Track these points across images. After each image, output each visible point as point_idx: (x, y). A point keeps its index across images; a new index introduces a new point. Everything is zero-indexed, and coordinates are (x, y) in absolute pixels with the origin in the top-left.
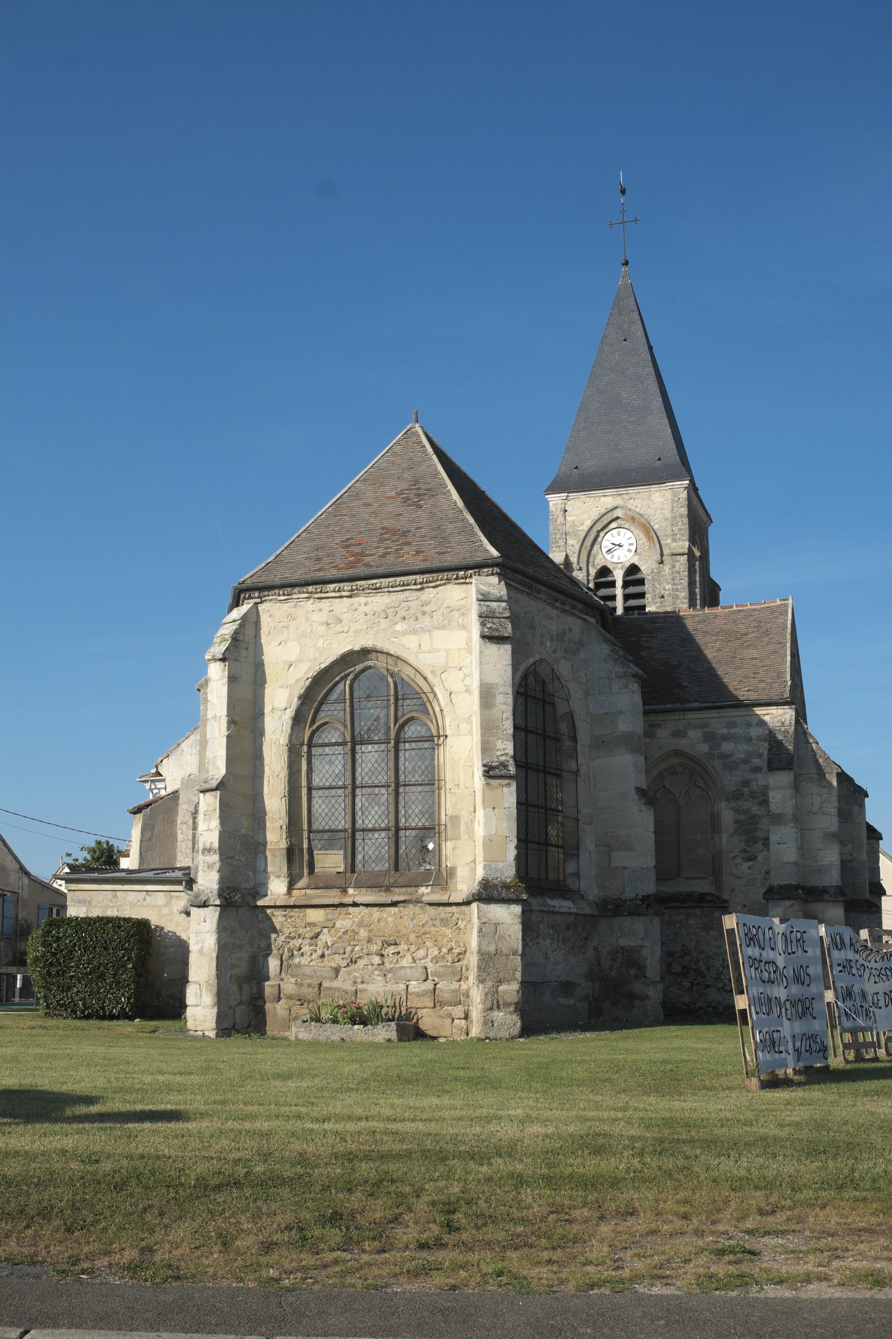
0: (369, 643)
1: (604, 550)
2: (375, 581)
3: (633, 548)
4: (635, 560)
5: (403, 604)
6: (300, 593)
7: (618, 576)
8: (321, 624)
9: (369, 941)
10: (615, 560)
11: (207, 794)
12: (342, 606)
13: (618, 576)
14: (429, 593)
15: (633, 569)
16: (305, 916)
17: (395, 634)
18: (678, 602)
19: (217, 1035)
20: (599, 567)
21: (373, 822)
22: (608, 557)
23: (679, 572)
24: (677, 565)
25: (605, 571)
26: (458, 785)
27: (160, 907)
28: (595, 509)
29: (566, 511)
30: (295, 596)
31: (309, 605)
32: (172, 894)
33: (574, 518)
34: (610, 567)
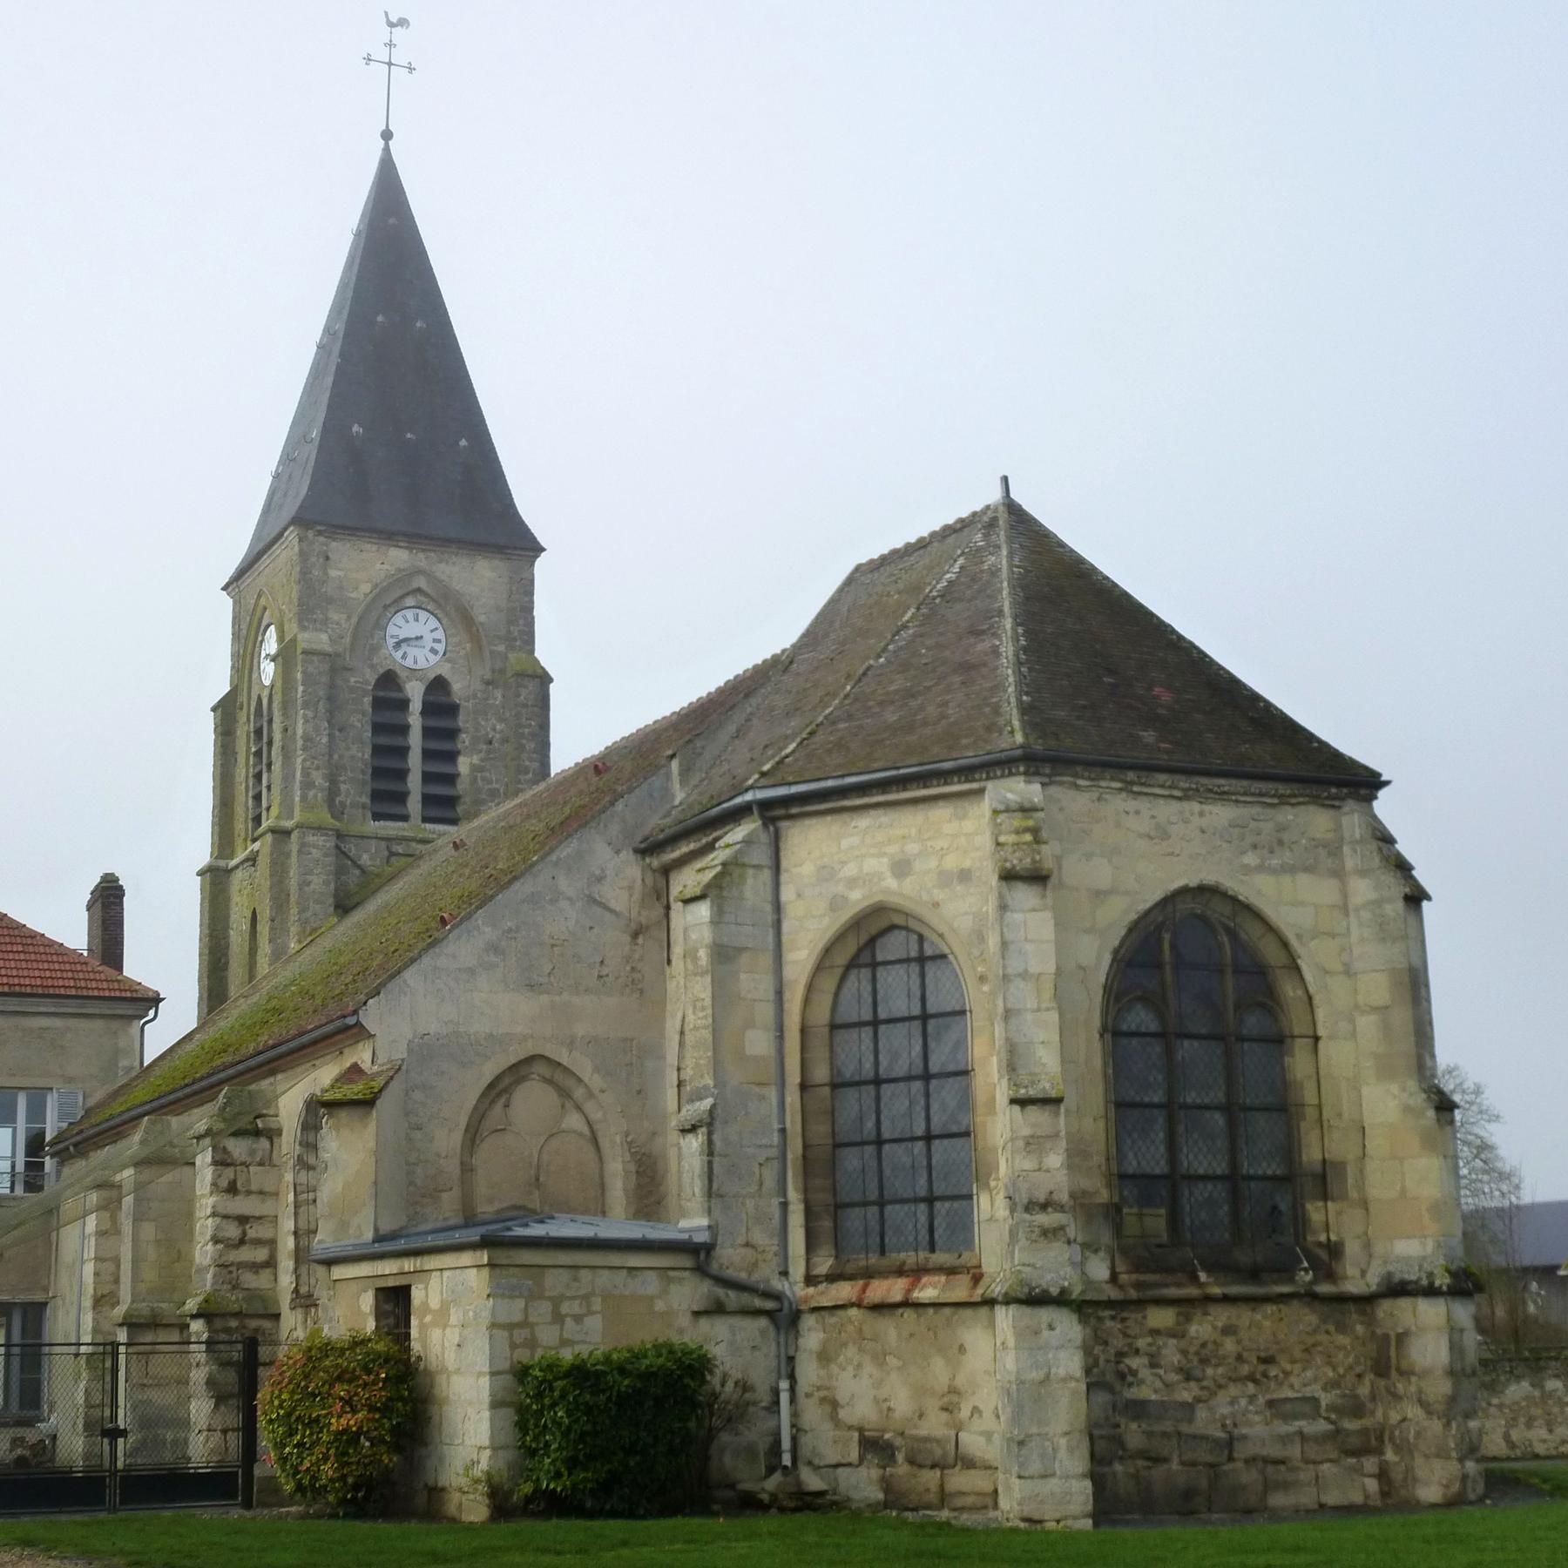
0: (1209, 878)
1: (391, 642)
2: (1222, 781)
3: (441, 648)
4: (445, 670)
5: (1253, 825)
6: (1112, 779)
7: (415, 692)
8: (1141, 836)
9: (1239, 1358)
10: (409, 663)
11: (1031, 1109)
12: (1168, 810)
13: (415, 692)
14: (1287, 815)
15: (438, 685)
16: (1145, 1317)
17: (1247, 870)
18: (524, 756)
19: (1096, 1525)
20: (381, 671)
21: (1205, 1164)
22: (398, 655)
23: (525, 706)
24: (524, 692)
25: (389, 679)
26: (1340, 1115)
27: (651, 1299)
28: (378, 566)
29: (327, 558)
30: (1103, 784)
31: (1120, 803)
32: (671, 1273)
33: (341, 573)
34: (403, 674)
